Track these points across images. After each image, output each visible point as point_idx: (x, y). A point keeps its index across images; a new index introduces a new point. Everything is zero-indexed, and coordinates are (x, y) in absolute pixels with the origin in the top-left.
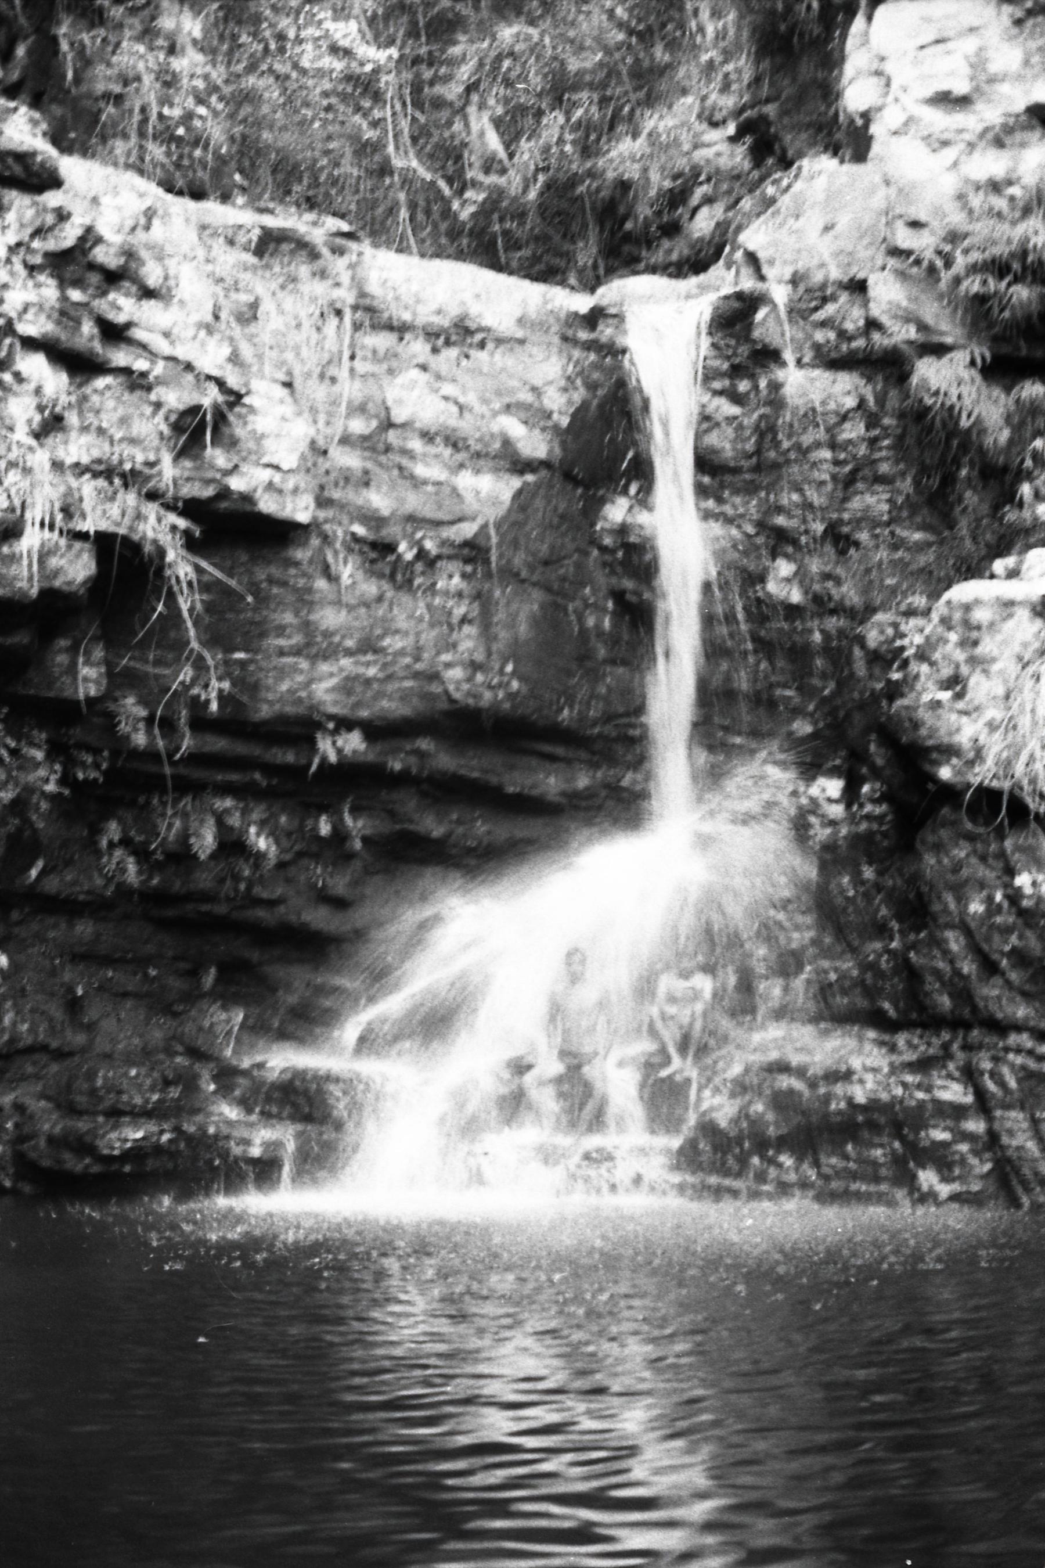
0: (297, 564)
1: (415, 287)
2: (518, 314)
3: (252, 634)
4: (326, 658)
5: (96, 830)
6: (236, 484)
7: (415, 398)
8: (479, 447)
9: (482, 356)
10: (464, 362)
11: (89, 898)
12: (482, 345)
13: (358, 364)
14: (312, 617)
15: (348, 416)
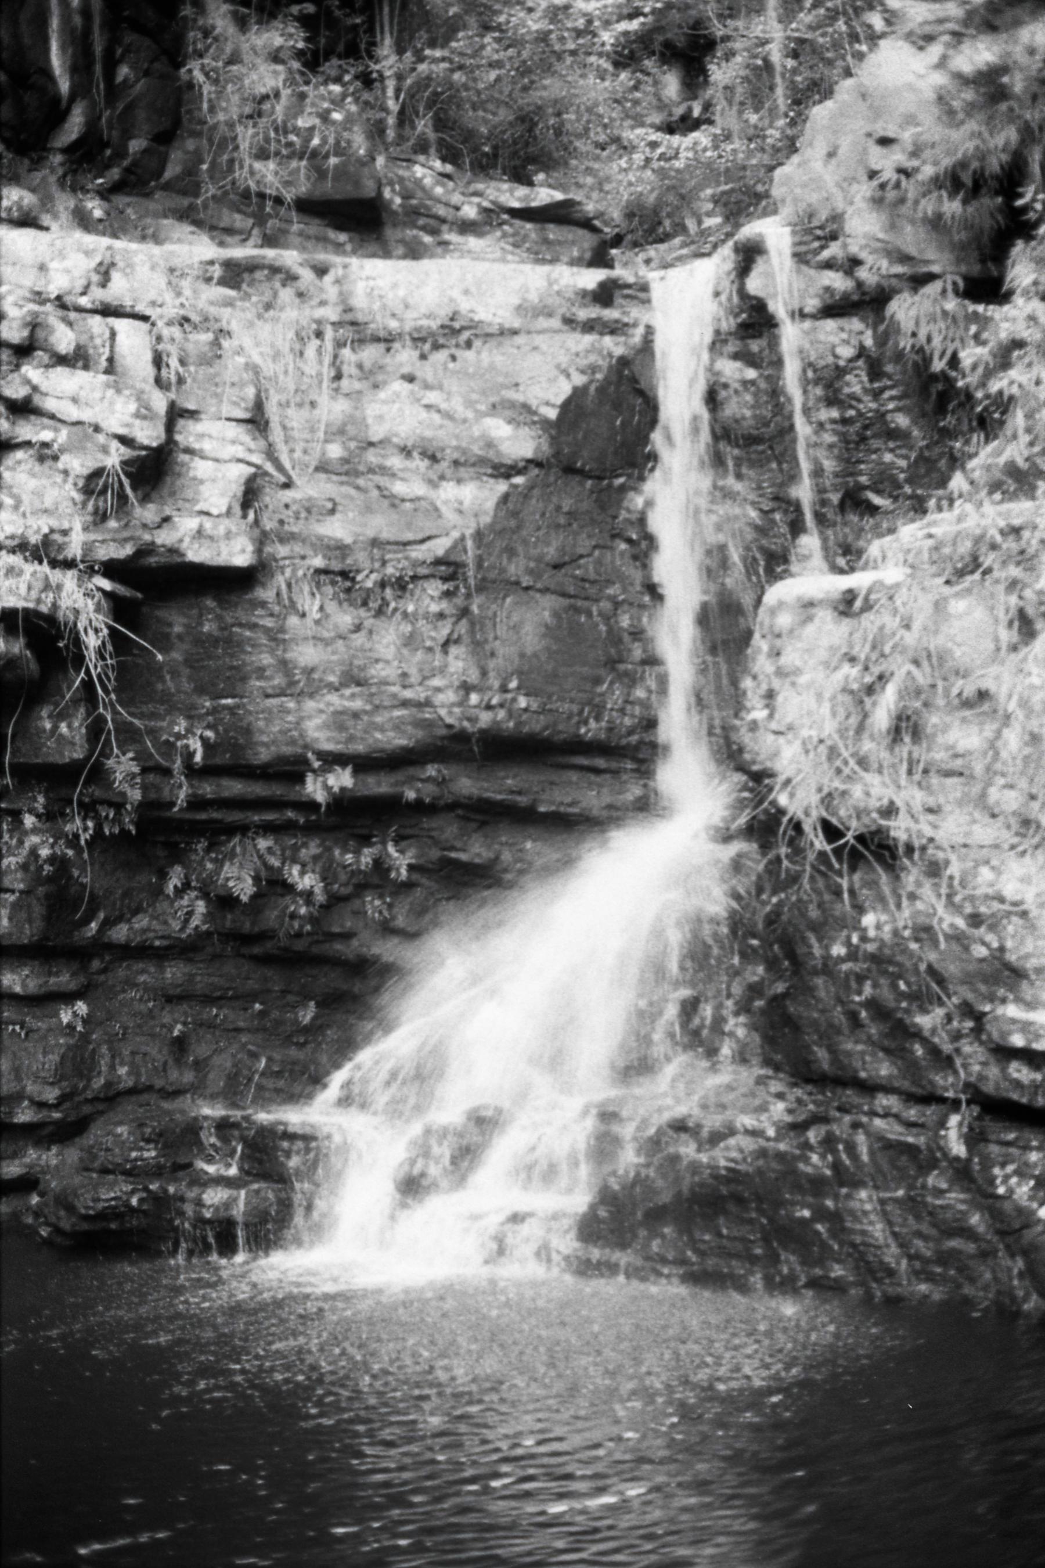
0: (263, 604)
1: (401, 293)
2: (516, 301)
3: (235, 680)
4: (311, 695)
5: (163, 876)
6: (164, 538)
7: (395, 413)
8: (456, 455)
9: (469, 355)
10: (451, 365)
11: (165, 943)
12: (469, 345)
13: (345, 383)
14: (289, 656)
15: (326, 441)
